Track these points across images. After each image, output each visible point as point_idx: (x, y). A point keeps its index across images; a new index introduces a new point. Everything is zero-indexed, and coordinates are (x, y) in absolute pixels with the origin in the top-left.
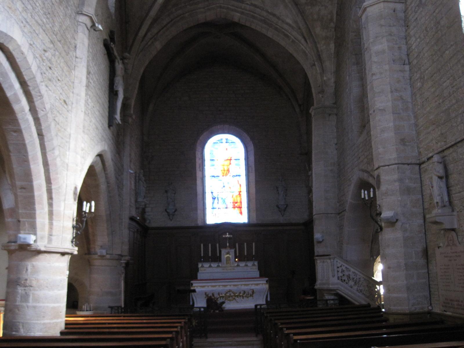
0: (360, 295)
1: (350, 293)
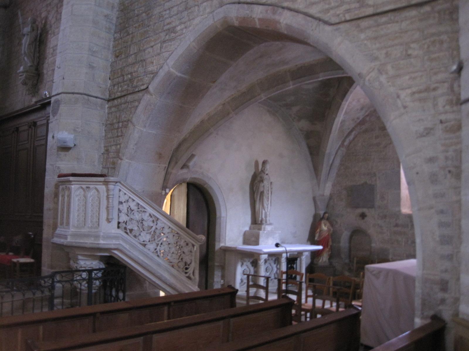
1: (141, 258)
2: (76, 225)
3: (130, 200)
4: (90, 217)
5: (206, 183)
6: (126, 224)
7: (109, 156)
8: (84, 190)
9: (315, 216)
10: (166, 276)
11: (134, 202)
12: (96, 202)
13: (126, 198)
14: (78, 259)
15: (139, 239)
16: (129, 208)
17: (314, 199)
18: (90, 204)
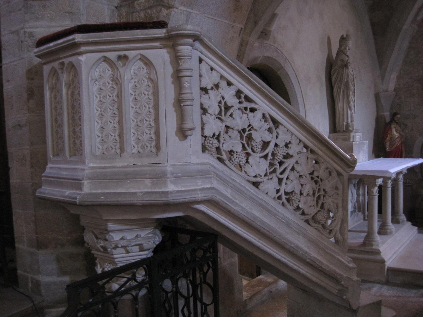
0: (287, 213)
2: (98, 153)
3: (223, 84)
4: (133, 130)
5: (281, 68)
6: (218, 138)
7: (134, 7)
8: (111, 67)
9: (379, 120)
10: (301, 243)
11: (232, 87)
12: (147, 93)
13: (215, 78)
14: (108, 231)
15: (246, 173)
16: (223, 103)
17: (377, 97)
18: (131, 98)
